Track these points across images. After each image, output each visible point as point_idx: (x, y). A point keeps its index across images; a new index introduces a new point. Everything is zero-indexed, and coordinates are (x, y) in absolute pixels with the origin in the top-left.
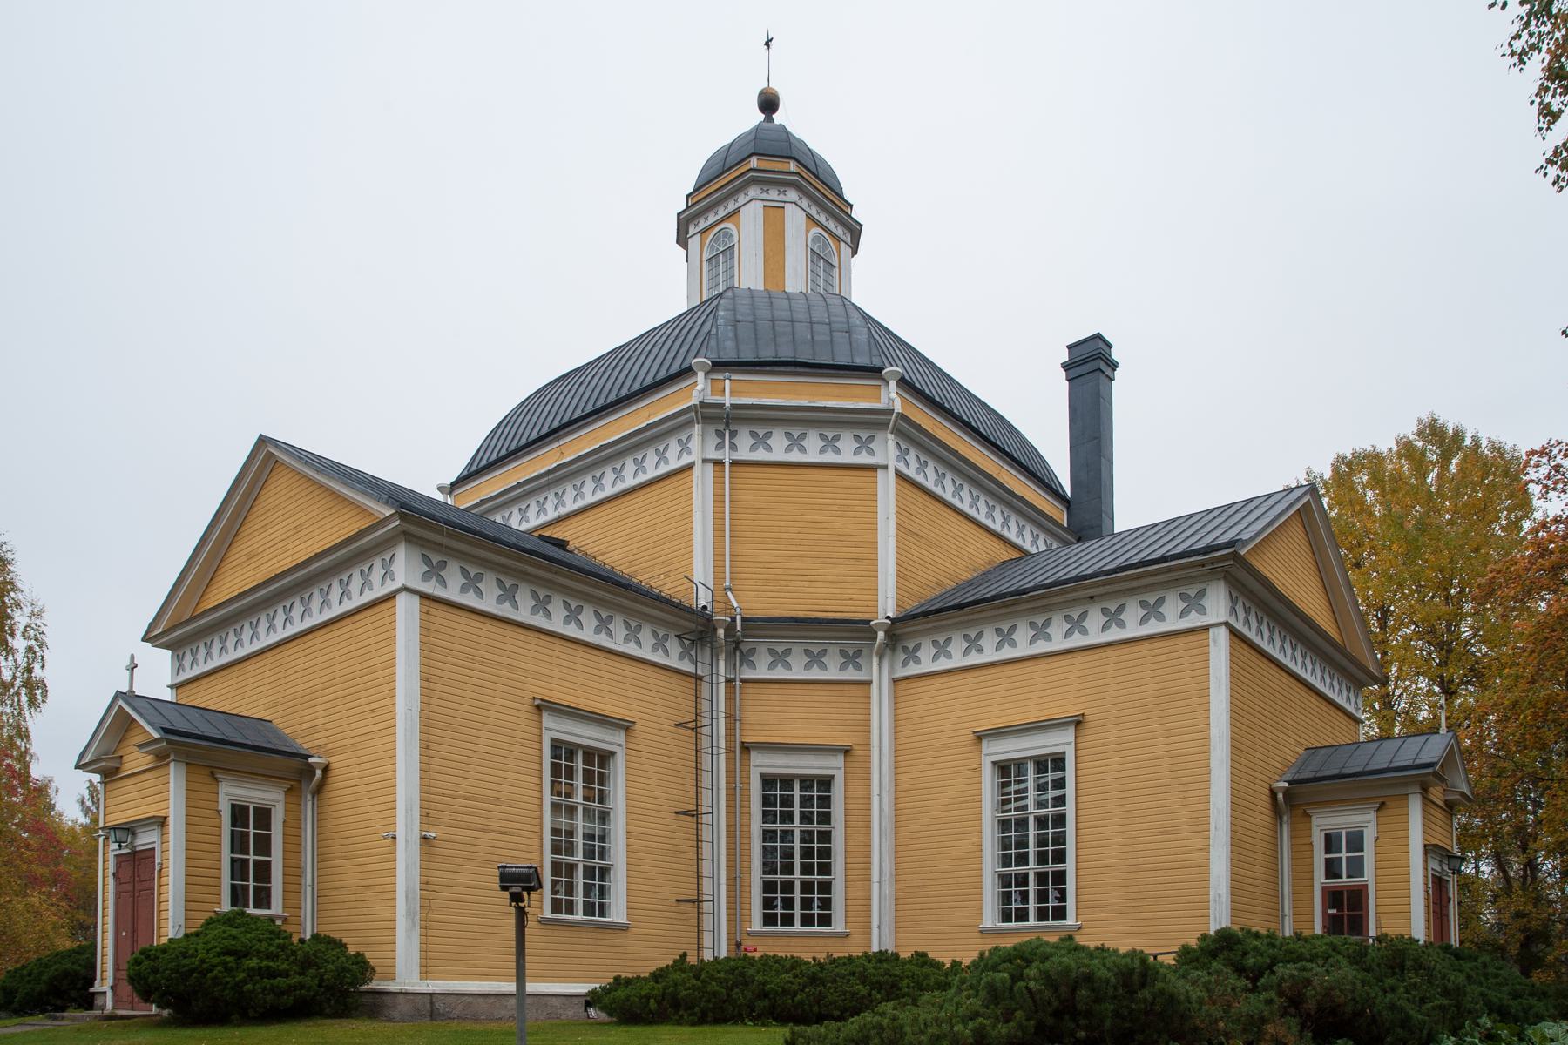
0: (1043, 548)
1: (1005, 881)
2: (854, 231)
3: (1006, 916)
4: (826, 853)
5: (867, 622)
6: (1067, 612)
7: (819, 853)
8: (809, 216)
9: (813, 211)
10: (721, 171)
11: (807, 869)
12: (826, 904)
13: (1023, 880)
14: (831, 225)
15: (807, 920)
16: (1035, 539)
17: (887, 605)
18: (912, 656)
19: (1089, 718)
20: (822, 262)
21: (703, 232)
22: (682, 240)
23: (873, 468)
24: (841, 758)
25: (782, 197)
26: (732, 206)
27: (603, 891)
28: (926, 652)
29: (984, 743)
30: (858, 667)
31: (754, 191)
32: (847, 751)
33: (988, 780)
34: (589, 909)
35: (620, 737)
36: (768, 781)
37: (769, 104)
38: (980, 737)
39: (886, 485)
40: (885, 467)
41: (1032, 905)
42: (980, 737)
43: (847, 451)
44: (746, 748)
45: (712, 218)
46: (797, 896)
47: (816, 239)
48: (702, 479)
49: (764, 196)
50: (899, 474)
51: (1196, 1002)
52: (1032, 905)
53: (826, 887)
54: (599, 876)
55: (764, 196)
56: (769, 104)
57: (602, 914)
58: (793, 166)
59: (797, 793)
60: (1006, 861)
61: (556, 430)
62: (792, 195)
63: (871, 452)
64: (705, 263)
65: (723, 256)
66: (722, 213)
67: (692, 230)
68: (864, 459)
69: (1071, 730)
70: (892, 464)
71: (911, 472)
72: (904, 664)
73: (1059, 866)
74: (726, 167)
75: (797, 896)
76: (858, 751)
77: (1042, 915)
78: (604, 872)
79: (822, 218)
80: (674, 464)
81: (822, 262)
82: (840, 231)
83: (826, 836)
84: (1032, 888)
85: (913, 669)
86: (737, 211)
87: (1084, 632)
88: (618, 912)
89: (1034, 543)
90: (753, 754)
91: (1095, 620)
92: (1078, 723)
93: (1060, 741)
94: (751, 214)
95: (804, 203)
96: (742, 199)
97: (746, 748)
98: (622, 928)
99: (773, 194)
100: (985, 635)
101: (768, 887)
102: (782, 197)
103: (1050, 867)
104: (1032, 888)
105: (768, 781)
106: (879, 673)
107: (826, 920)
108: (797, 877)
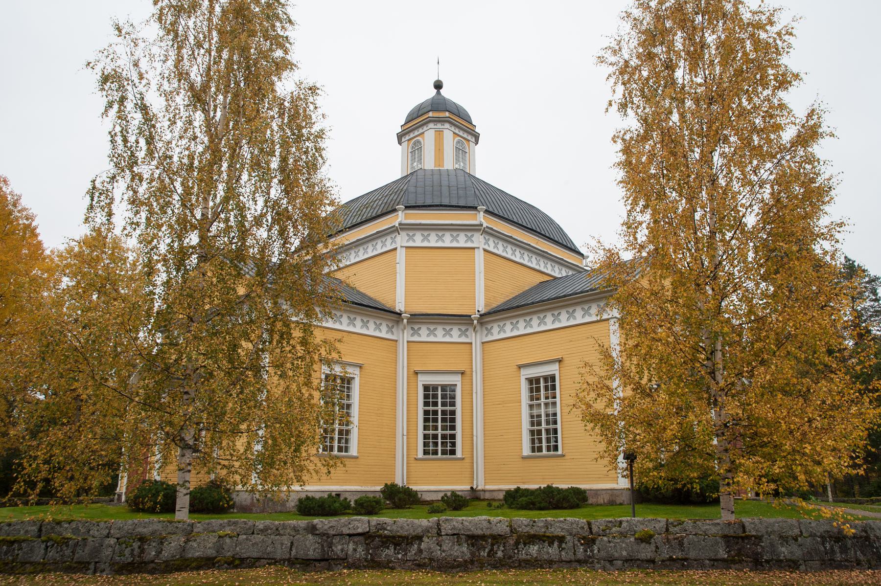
0: (564, 274)
1: (532, 432)
2: (477, 137)
3: (533, 450)
4: (426, 420)
5: (470, 316)
6: (538, 315)
7: (450, 419)
8: (454, 133)
9: (457, 131)
10: (415, 116)
11: (444, 404)
12: (454, 444)
13: (539, 432)
14: (465, 136)
15: (444, 452)
16: (560, 270)
17: (481, 305)
18: (489, 331)
19: (565, 359)
20: (461, 152)
21: (409, 140)
22: (400, 143)
23: (474, 248)
24: (460, 376)
25: (443, 127)
26: (421, 131)
27: (347, 441)
28: (495, 330)
29: (522, 369)
30: (467, 336)
31: (431, 125)
32: (463, 373)
33: (524, 387)
34: (340, 449)
35: (357, 371)
36: (426, 388)
37: (438, 86)
38: (520, 367)
39: (479, 256)
40: (479, 248)
41: (544, 444)
42: (520, 367)
43: (462, 241)
44: (416, 373)
45: (412, 135)
46: (440, 441)
47: (458, 142)
48: (401, 255)
49: (435, 127)
50: (485, 250)
51: (386, 498)
52: (544, 444)
53: (453, 437)
54: (345, 434)
55: (435, 127)
56: (438, 86)
57: (346, 451)
58: (447, 114)
59: (440, 393)
60: (532, 424)
61: (358, 224)
62: (447, 125)
63: (472, 242)
64: (409, 154)
65: (416, 150)
66: (416, 133)
67: (403, 140)
68: (469, 245)
69: (557, 364)
70: (482, 246)
71: (491, 249)
72: (486, 336)
73: (427, 408)
74: (419, 114)
75: (440, 441)
76: (468, 372)
77: (549, 449)
78: (348, 432)
79: (461, 133)
80: (389, 248)
81: (461, 152)
82: (469, 138)
83: (453, 413)
84: (544, 436)
85: (490, 338)
86: (423, 133)
87: (505, 332)
88: (353, 451)
89: (560, 273)
90: (419, 376)
91: (508, 327)
92: (560, 361)
93: (553, 369)
94: (429, 136)
95: (453, 129)
96: (425, 128)
97: (416, 373)
98: (356, 458)
99: (439, 126)
100: (533, 320)
101: (426, 437)
102: (443, 127)
103: (551, 426)
104: (544, 436)
105: (426, 388)
106: (476, 338)
107: (453, 452)
108: (440, 408)
